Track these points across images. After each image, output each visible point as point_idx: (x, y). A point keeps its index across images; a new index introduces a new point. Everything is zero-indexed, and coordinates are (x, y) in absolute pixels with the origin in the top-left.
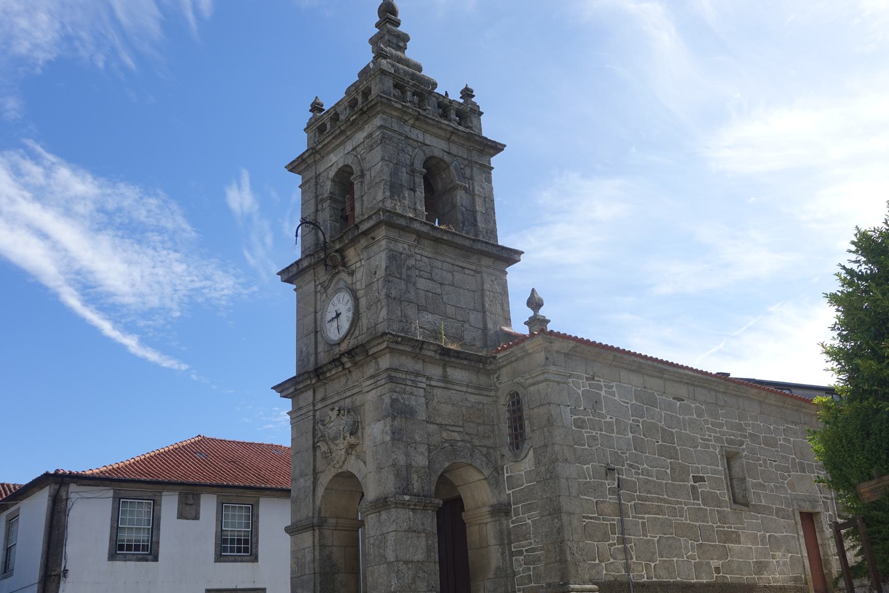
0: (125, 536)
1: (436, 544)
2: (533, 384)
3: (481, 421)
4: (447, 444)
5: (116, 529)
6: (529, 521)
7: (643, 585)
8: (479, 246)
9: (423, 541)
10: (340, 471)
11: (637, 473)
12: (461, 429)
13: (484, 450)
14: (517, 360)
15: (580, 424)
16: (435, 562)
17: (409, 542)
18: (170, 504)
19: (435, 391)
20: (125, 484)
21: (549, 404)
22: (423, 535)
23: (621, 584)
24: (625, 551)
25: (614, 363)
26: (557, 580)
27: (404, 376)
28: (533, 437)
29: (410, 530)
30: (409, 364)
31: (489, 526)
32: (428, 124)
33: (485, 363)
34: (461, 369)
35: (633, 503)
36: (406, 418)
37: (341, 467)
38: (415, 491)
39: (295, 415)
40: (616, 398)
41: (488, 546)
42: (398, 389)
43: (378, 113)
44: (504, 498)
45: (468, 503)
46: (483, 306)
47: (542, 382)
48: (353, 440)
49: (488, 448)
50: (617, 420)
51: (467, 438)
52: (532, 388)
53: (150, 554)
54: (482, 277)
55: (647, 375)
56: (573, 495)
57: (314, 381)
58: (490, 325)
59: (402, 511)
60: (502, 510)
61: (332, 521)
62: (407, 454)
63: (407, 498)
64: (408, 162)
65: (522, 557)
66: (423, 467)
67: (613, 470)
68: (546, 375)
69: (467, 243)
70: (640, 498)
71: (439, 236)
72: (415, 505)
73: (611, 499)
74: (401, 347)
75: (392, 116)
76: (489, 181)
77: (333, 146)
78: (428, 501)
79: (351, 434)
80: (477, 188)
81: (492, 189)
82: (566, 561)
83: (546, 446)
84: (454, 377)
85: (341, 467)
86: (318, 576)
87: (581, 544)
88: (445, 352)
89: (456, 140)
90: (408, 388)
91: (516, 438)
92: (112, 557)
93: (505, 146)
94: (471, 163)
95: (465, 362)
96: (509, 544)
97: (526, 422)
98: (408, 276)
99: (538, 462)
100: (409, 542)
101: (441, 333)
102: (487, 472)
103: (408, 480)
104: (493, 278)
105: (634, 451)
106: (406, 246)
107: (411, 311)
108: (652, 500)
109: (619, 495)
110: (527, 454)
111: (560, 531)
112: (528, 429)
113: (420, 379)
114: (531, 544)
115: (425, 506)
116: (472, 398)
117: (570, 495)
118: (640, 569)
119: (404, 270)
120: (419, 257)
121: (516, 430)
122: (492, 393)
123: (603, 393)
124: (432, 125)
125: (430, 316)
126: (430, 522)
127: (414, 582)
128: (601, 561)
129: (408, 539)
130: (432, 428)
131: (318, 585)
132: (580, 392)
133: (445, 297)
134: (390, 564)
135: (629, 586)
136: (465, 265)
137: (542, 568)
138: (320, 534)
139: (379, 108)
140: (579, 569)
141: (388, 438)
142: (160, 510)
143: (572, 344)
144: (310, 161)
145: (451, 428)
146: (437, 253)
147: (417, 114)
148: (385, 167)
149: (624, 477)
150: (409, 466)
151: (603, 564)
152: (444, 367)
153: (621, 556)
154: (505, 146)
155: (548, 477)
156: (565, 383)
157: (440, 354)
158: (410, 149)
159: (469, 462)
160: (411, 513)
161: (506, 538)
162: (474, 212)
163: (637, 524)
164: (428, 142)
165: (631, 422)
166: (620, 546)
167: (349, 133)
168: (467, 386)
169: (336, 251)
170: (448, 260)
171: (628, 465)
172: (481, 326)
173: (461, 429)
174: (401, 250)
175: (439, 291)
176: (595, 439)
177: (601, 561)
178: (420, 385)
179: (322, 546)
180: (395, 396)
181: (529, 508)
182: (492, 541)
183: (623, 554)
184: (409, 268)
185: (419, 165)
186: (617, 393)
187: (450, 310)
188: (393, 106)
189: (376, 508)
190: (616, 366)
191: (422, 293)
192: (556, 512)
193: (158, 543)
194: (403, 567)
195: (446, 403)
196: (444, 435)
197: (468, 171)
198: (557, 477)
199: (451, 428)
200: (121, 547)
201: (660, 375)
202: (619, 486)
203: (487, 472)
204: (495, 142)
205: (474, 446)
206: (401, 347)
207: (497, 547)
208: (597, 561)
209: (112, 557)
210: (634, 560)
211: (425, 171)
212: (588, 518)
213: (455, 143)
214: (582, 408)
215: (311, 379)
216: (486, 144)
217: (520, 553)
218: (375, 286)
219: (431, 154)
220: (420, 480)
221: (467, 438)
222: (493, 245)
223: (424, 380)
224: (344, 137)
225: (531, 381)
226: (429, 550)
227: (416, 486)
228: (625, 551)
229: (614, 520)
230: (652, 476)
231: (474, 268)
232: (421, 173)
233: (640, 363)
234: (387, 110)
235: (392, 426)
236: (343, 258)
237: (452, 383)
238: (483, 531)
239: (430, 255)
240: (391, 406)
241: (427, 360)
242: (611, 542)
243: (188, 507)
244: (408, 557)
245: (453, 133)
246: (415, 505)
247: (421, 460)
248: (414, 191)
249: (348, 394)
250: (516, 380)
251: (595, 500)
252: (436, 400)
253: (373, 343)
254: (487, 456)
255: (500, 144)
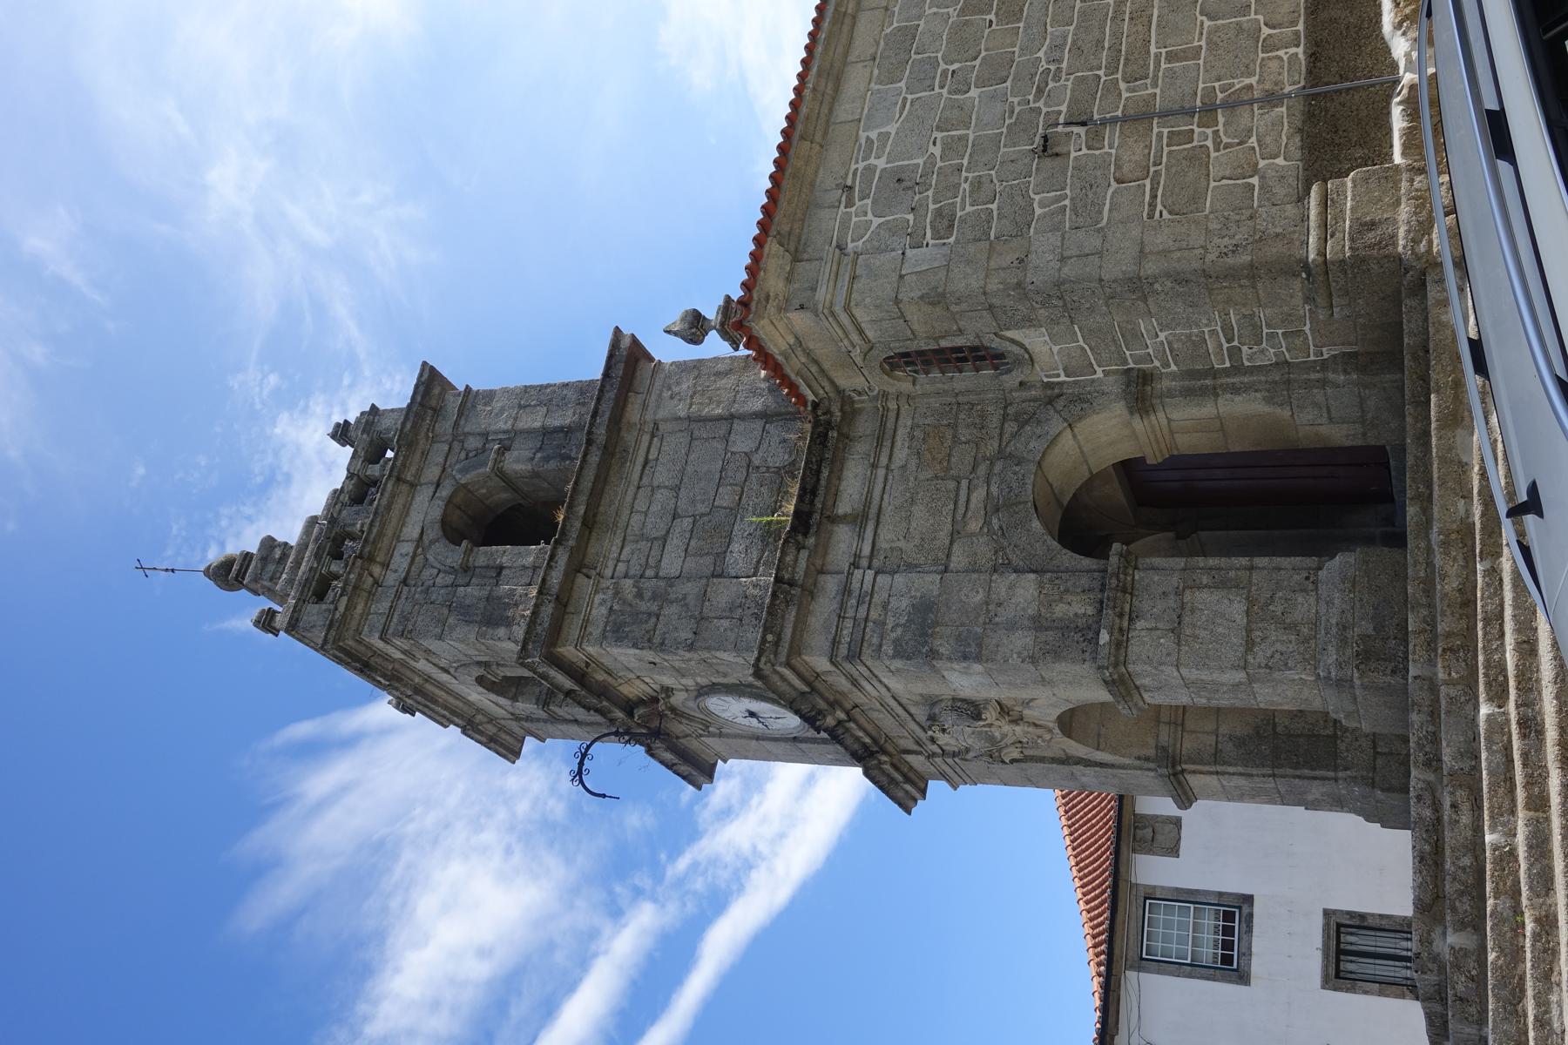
0: (1208, 951)
1: (1212, 562)
2: (861, 332)
3: (949, 434)
4: (995, 521)
5: (1194, 969)
6: (1162, 336)
7: (1313, 57)
8: (601, 432)
9: (1203, 596)
10: (1057, 731)
11: (1057, 78)
12: (964, 483)
13: (1011, 427)
14: (816, 362)
15: (945, 222)
16: (1251, 568)
17: (1203, 634)
18: (1151, 870)
19: (883, 544)
20: (1117, 951)
21: (897, 301)
22: (1188, 596)
23: (1310, 116)
24: (1231, 105)
25: (818, 138)
26: (1297, 284)
27: (849, 624)
28: (976, 329)
29: (1176, 631)
30: (824, 608)
31: (1175, 415)
32: (381, 534)
33: (829, 425)
34: (839, 479)
35: (1122, 85)
36: (936, 623)
37: (1050, 731)
38: (1090, 611)
39: (956, 778)
40: (892, 128)
41: (1218, 417)
42: (875, 640)
43: (360, 642)
44: (1113, 386)
45: (1126, 451)
46: (720, 418)
47: (852, 316)
48: (990, 715)
49: (1005, 417)
50: (939, 129)
51: (982, 469)
52: (870, 334)
53: (1240, 908)
54: (665, 420)
55: (846, 54)
56: (1098, 243)
57: (884, 758)
58: (757, 405)
59: (1134, 649)
60: (1140, 390)
61: (1164, 738)
62: (1012, 626)
63: (1104, 637)
64: (449, 579)
65: (1245, 349)
66: (1041, 586)
67: (1045, 138)
68: (838, 309)
69: (594, 459)
70: (1112, 68)
71: (578, 524)
72: (1121, 616)
73: (1112, 136)
74: (788, 632)
75: (366, 614)
76: (490, 396)
77: (451, 700)
78: (1114, 582)
79: (977, 716)
80: (501, 425)
81: (505, 391)
82: (1251, 265)
83: (991, 308)
84: (856, 497)
85: (1050, 731)
86: (1277, 771)
87: (1214, 226)
88: (802, 521)
89: (413, 470)
90: (874, 615)
91: (983, 358)
92: (1243, 977)
93: (425, 364)
94: (458, 437)
95: (825, 473)
96: (1213, 373)
97: (944, 344)
98: (654, 597)
99: (1029, 322)
100: (1203, 634)
101: (769, 523)
102: (1056, 425)
103: (1066, 627)
104: (666, 394)
105: (1008, 83)
106: (598, 598)
107: (723, 594)
108: (1117, 35)
109: (1104, 122)
110: (1013, 341)
111: (1180, 279)
112: (960, 341)
113: (856, 585)
114: (1213, 332)
115: (1124, 591)
116: (901, 454)
117: (1100, 254)
118: (1274, 65)
119: (643, 606)
120: (621, 567)
121: (965, 360)
122: (892, 405)
123: (881, 163)
124: (383, 525)
125: (736, 547)
126: (1160, 574)
127: (1292, 627)
128: (1255, 171)
129: (1197, 637)
130: (959, 559)
131: (1298, 773)
132: (876, 221)
133: (701, 508)
134: (1251, 680)
135: (1314, 96)
136: (640, 460)
137: (1268, 311)
138: (1192, 761)
139: (351, 642)
140: (1272, 231)
141: (977, 667)
142: (1163, 888)
143: (772, 246)
144: (491, 730)
145: (961, 510)
146: (615, 524)
147: (359, 562)
148: (454, 635)
149: (1064, 108)
150: (1038, 624)
151: (1262, 163)
152: (834, 520)
153: (1243, 117)
154: (425, 364)
155: (1061, 303)
156: (855, 262)
157: (805, 535)
158: (427, 573)
159: (1033, 467)
160: (1140, 624)
161: (1202, 381)
162: (546, 432)
163: (1171, 74)
164: (416, 535)
165: (945, 91)
166: (1221, 119)
167: (417, 680)
168: (874, 466)
169: (630, 714)
170: (629, 498)
171: (1038, 97)
172: (759, 424)
173: (964, 483)
174: (604, 610)
175: (686, 523)
176: (977, 185)
177: (1255, 171)
178: (867, 586)
179: (1217, 757)
180: (888, 648)
181: (1134, 337)
182: (1207, 410)
183: (1239, 110)
184: (639, 595)
185: (454, 555)
186: (881, 129)
187: (726, 498)
188: (344, 615)
189: (1129, 694)
190: (826, 133)
191: (691, 564)
192: (1138, 286)
193: (1221, 894)
194: (1261, 655)
195: (908, 519)
196: (974, 526)
197: (473, 443)
198: (1058, 284)
199: (961, 510)
200: (1227, 960)
201: (848, 21)
202: (1083, 124)
203: (1056, 425)
204: (417, 387)
205: (1001, 454)
206: (788, 632)
207: (1220, 401)
208: (1255, 180)
209: (1243, 977)
210: (1253, 80)
211: (464, 543)
212: (1152, 206)
213: (420, 470)
214: (911, 217)
215: (880, 762)
216: (421, 404)
217: (1234, 353)
218: (677, 664)
219: (437, 526)
220: (1069, 598)
221: (982, 469)
222: (601, 390)
223: (858, 573)
224: (428, 686)
225: (855, 337)
226: (1222, 585)
227: (1078, 607)
228: (1231, 105)
229: (1160, 135)
230: (1065, 38)
231: (646, 438)
232: (468, 553)
233: (819, 74)
234: (354, 625)
235: (949, 659)
236: (641, 702)
237: (867, 503)
238: (1185, 426)
239: (618, 541)
240: (908, 658)
241: (819, 562)
242: (1209, 143)
243: (1159, 837)
244: (1237, 640)
245: (398, 479)
246: (1121, 616)
247: (1024, 592)
248: (501, 569)
249: (900, 711)
250: (859, 360)
251: (1114, 185)
252: (902, 544)
253: (783, 687)
254: (1024, 420)
255: (421, 375)
